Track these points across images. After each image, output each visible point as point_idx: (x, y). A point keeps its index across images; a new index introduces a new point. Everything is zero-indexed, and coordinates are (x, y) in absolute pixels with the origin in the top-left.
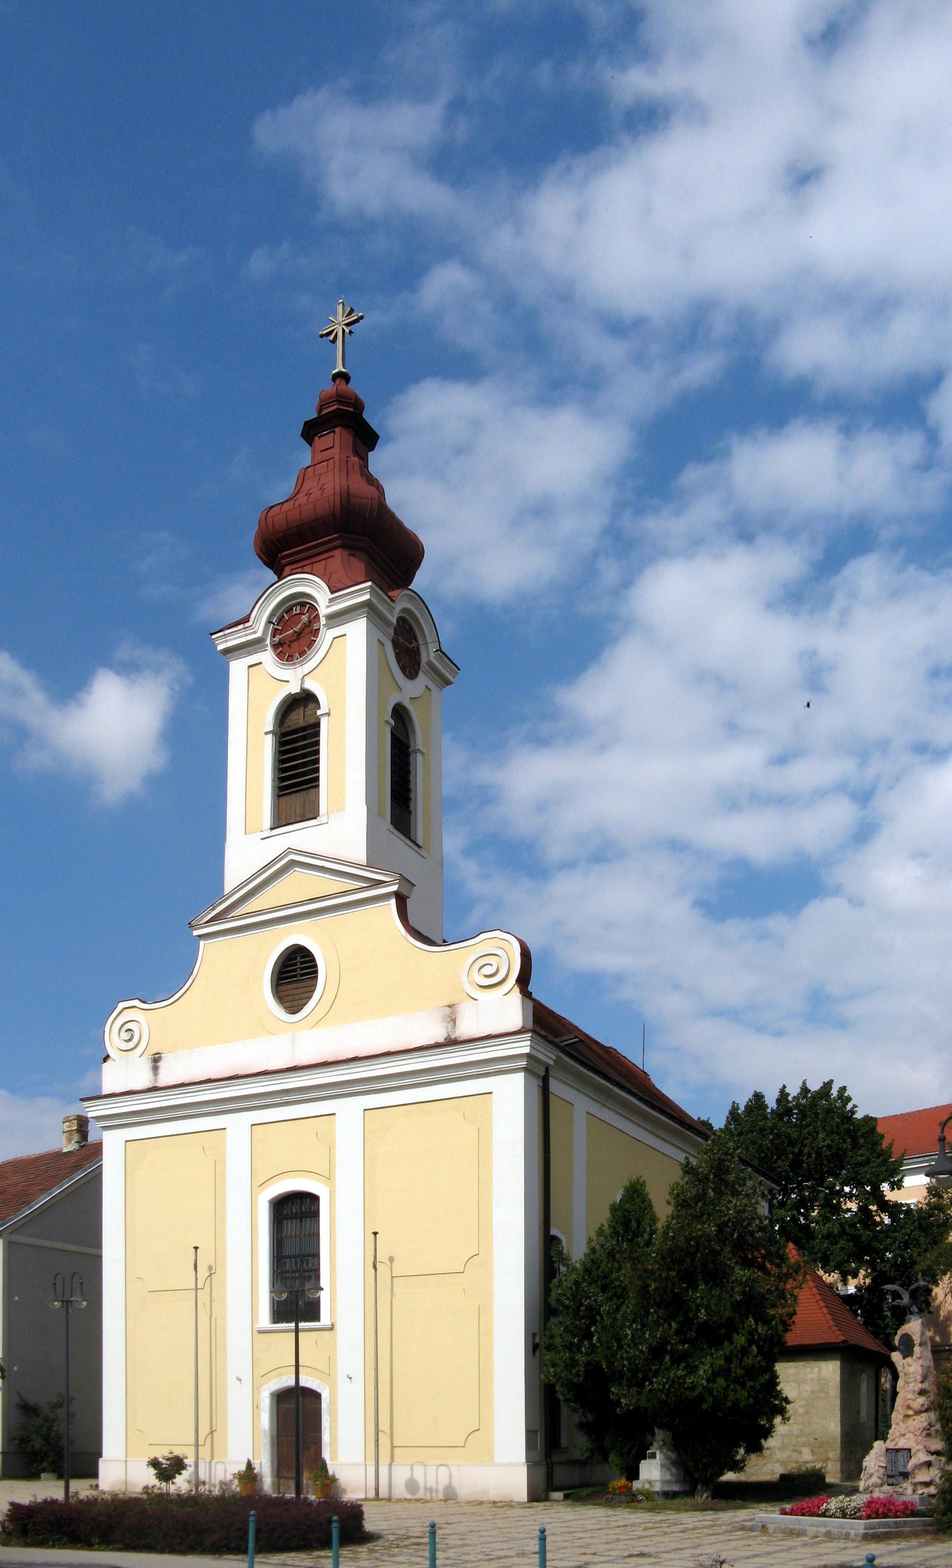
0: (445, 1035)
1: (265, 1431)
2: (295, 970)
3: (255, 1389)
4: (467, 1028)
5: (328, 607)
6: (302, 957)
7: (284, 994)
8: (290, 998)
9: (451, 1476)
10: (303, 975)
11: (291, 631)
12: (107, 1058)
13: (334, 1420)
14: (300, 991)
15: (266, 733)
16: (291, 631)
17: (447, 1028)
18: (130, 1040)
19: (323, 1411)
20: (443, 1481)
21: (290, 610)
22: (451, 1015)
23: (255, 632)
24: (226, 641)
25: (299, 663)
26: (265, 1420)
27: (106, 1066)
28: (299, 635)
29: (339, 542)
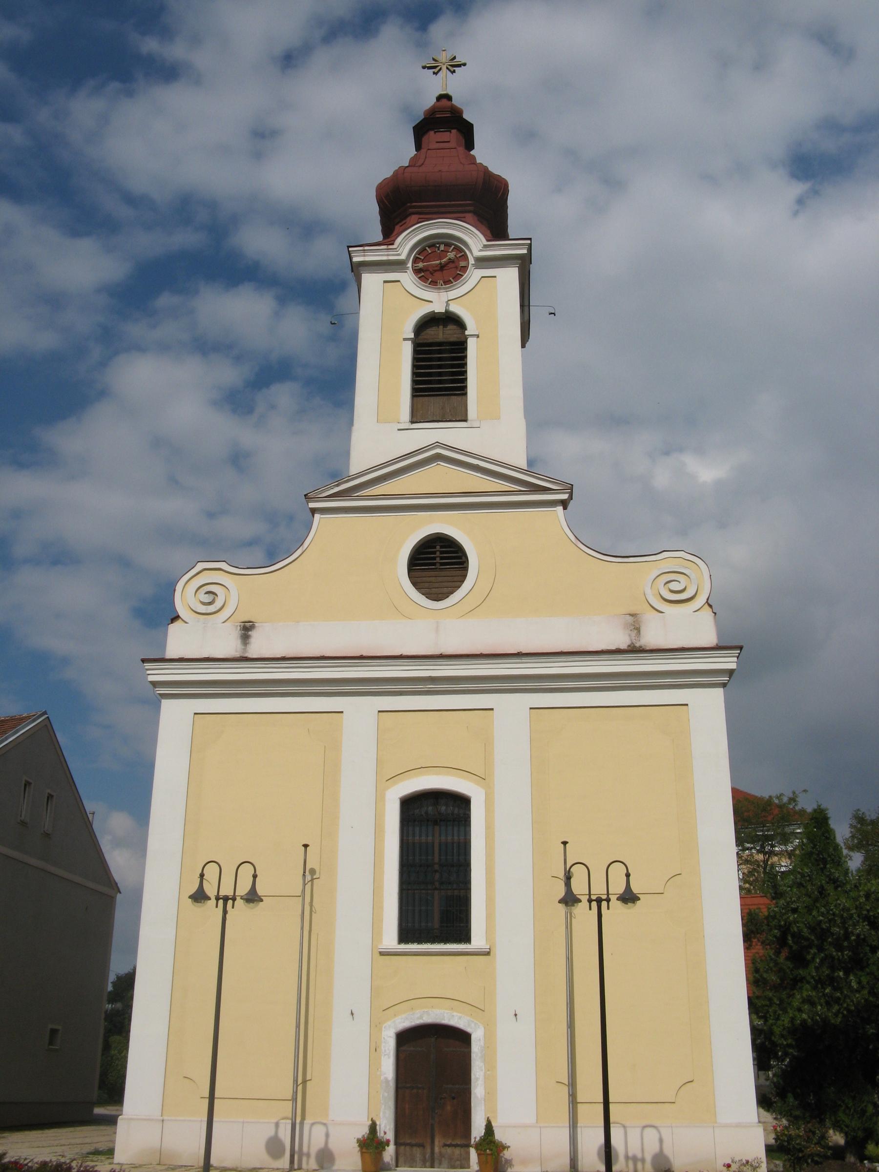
0: (629, 643)
1: (387, 1081)
2: (434, 558)
3: (376, 1026)
4: (652, 637)
5: (481, 250)
6: (441, 547)
7: (419, 580)
8: (426, 585)
9: (661, 1141)
10: (442, 564)
11: (438, 262)
12: (177, 618)
13: (491, 1066)
14: (440, 579)
15: (405, 339)
16: (438, 262)
17: (630, 635)
18: (210, 603)
19: (473, 1056)
20: (651, 1148)
21: (432, 246)
22: (635, 624)
23: (399, 255)
24: (364, 256)
25: (444, 288)
26: (388, 1067)
27: (174, 629)
28: (442, 267)
29: (471, 208)
